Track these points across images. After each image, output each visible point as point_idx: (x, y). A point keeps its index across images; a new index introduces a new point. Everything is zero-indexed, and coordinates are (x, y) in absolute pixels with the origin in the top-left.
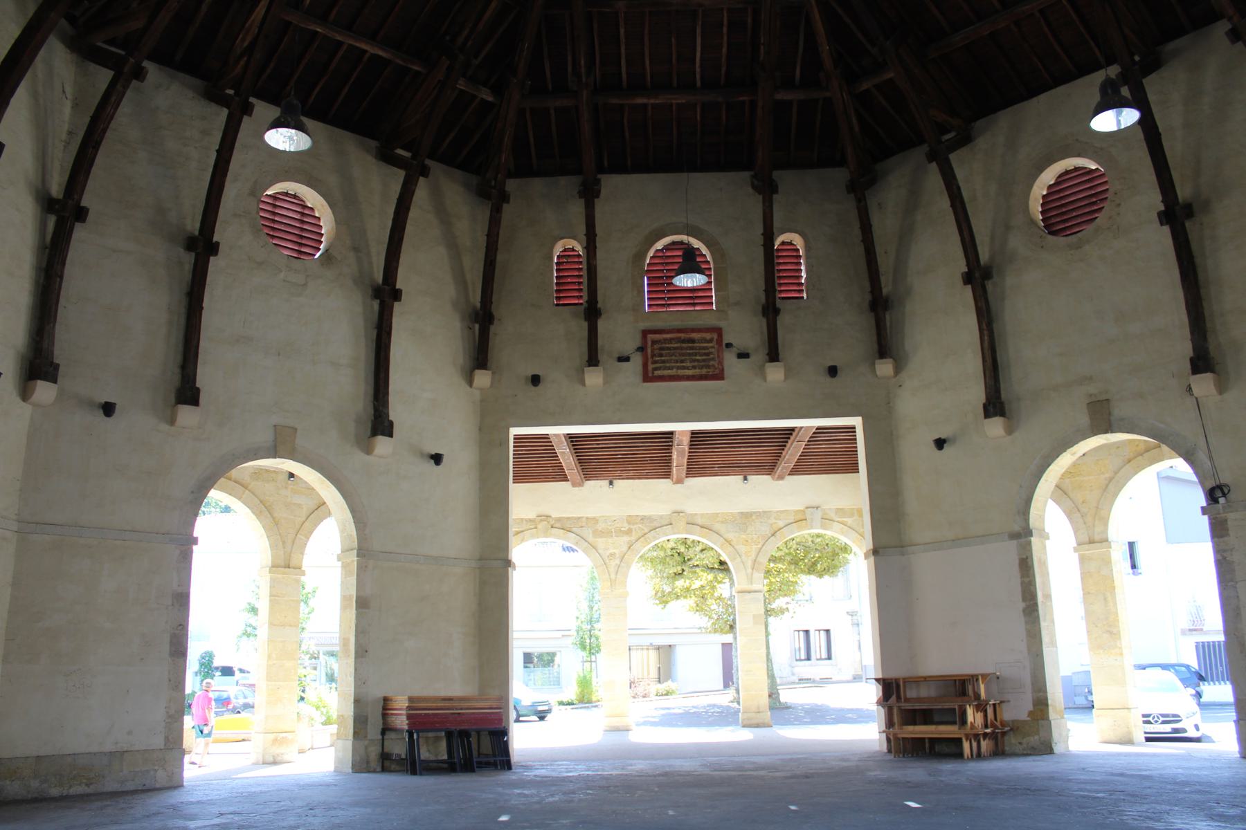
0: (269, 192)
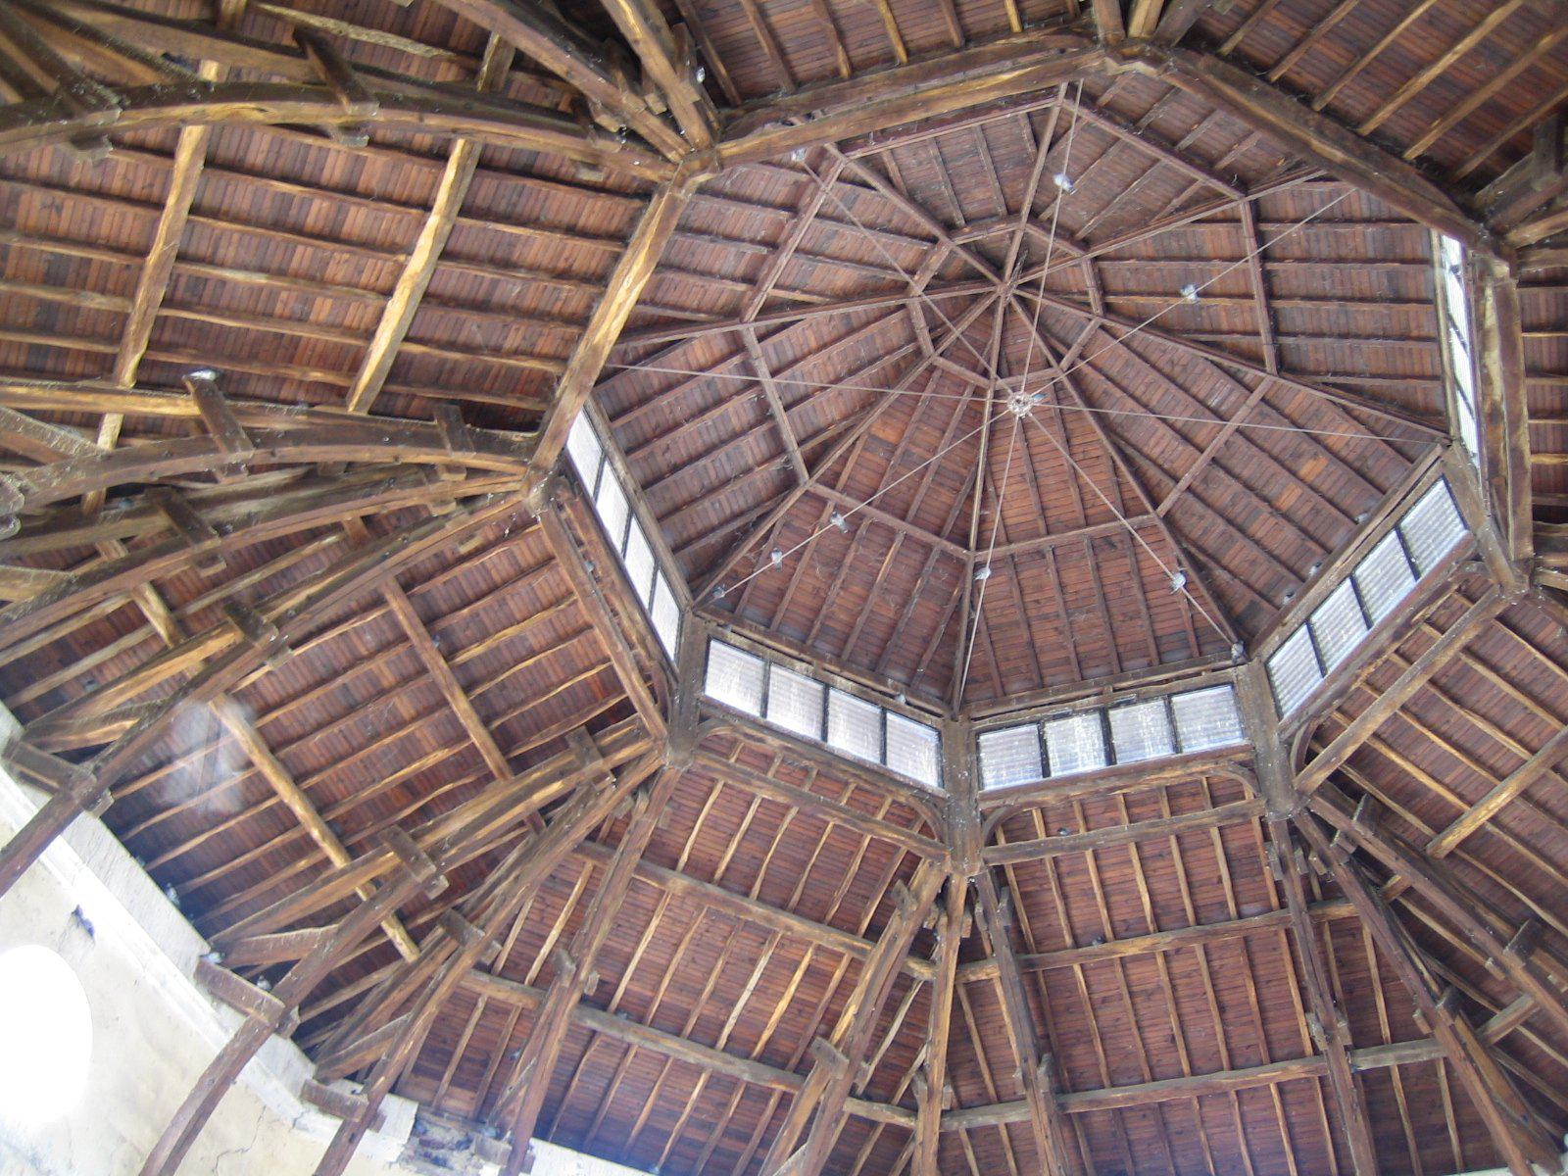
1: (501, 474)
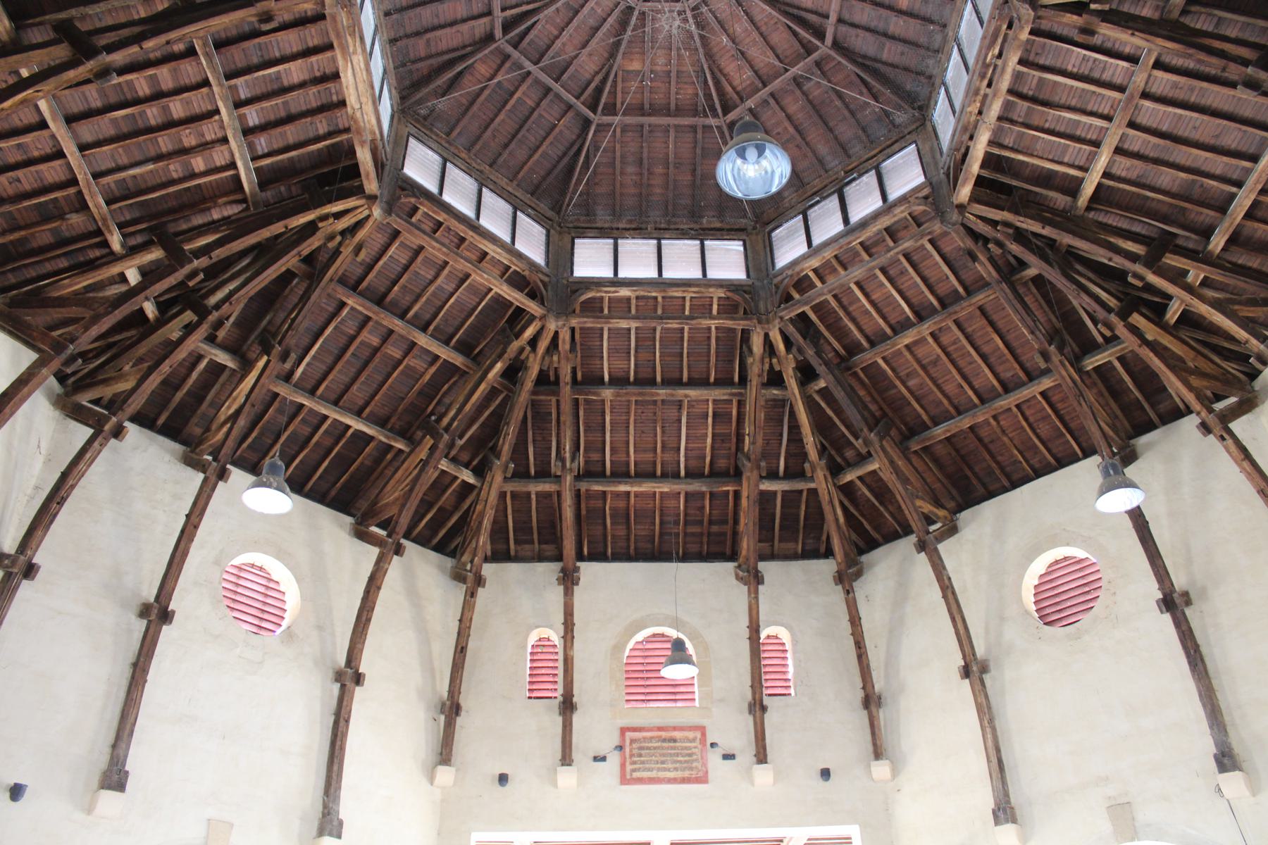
0: (236, 561)
1: (356, 208)
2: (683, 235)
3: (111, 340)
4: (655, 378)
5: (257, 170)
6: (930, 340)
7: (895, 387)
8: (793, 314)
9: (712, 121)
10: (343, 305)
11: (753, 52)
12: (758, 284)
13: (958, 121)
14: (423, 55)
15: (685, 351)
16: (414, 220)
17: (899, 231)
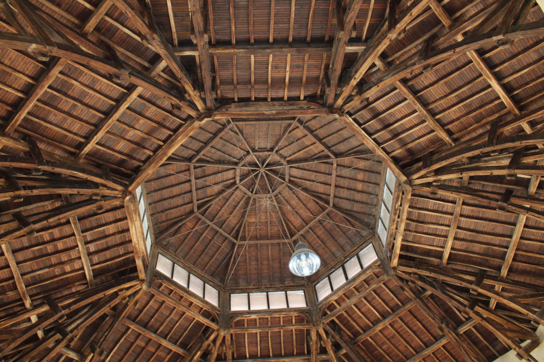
1: (135, 285)
2: (278, 289)
3: (20, 349)
4: (269, 355)
5: (93, 270)
6: (389, 327)
7: (377, 349)
8: (328, 321)
9: (286, 241)
10: (129, 328)
11: (301, 212)
12: (311, 309)
13: (388, 233)
14: (164, 220)
15: (282, 341)
16: (160, 289)
17: (369, 281)
